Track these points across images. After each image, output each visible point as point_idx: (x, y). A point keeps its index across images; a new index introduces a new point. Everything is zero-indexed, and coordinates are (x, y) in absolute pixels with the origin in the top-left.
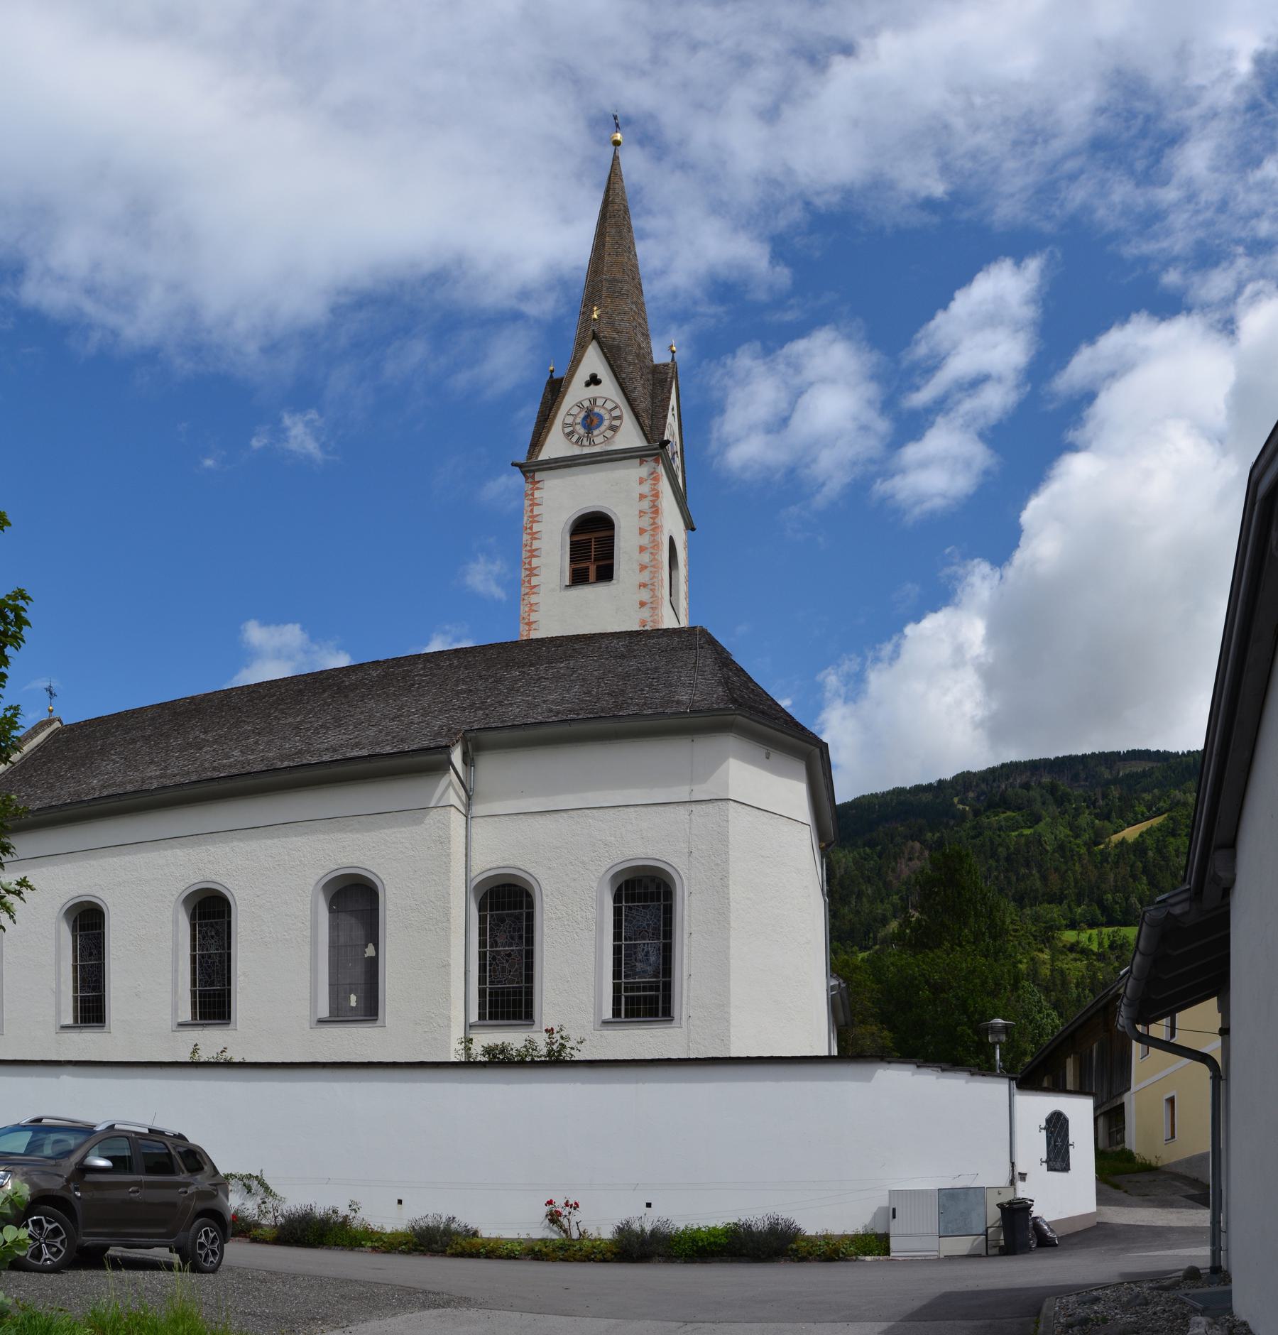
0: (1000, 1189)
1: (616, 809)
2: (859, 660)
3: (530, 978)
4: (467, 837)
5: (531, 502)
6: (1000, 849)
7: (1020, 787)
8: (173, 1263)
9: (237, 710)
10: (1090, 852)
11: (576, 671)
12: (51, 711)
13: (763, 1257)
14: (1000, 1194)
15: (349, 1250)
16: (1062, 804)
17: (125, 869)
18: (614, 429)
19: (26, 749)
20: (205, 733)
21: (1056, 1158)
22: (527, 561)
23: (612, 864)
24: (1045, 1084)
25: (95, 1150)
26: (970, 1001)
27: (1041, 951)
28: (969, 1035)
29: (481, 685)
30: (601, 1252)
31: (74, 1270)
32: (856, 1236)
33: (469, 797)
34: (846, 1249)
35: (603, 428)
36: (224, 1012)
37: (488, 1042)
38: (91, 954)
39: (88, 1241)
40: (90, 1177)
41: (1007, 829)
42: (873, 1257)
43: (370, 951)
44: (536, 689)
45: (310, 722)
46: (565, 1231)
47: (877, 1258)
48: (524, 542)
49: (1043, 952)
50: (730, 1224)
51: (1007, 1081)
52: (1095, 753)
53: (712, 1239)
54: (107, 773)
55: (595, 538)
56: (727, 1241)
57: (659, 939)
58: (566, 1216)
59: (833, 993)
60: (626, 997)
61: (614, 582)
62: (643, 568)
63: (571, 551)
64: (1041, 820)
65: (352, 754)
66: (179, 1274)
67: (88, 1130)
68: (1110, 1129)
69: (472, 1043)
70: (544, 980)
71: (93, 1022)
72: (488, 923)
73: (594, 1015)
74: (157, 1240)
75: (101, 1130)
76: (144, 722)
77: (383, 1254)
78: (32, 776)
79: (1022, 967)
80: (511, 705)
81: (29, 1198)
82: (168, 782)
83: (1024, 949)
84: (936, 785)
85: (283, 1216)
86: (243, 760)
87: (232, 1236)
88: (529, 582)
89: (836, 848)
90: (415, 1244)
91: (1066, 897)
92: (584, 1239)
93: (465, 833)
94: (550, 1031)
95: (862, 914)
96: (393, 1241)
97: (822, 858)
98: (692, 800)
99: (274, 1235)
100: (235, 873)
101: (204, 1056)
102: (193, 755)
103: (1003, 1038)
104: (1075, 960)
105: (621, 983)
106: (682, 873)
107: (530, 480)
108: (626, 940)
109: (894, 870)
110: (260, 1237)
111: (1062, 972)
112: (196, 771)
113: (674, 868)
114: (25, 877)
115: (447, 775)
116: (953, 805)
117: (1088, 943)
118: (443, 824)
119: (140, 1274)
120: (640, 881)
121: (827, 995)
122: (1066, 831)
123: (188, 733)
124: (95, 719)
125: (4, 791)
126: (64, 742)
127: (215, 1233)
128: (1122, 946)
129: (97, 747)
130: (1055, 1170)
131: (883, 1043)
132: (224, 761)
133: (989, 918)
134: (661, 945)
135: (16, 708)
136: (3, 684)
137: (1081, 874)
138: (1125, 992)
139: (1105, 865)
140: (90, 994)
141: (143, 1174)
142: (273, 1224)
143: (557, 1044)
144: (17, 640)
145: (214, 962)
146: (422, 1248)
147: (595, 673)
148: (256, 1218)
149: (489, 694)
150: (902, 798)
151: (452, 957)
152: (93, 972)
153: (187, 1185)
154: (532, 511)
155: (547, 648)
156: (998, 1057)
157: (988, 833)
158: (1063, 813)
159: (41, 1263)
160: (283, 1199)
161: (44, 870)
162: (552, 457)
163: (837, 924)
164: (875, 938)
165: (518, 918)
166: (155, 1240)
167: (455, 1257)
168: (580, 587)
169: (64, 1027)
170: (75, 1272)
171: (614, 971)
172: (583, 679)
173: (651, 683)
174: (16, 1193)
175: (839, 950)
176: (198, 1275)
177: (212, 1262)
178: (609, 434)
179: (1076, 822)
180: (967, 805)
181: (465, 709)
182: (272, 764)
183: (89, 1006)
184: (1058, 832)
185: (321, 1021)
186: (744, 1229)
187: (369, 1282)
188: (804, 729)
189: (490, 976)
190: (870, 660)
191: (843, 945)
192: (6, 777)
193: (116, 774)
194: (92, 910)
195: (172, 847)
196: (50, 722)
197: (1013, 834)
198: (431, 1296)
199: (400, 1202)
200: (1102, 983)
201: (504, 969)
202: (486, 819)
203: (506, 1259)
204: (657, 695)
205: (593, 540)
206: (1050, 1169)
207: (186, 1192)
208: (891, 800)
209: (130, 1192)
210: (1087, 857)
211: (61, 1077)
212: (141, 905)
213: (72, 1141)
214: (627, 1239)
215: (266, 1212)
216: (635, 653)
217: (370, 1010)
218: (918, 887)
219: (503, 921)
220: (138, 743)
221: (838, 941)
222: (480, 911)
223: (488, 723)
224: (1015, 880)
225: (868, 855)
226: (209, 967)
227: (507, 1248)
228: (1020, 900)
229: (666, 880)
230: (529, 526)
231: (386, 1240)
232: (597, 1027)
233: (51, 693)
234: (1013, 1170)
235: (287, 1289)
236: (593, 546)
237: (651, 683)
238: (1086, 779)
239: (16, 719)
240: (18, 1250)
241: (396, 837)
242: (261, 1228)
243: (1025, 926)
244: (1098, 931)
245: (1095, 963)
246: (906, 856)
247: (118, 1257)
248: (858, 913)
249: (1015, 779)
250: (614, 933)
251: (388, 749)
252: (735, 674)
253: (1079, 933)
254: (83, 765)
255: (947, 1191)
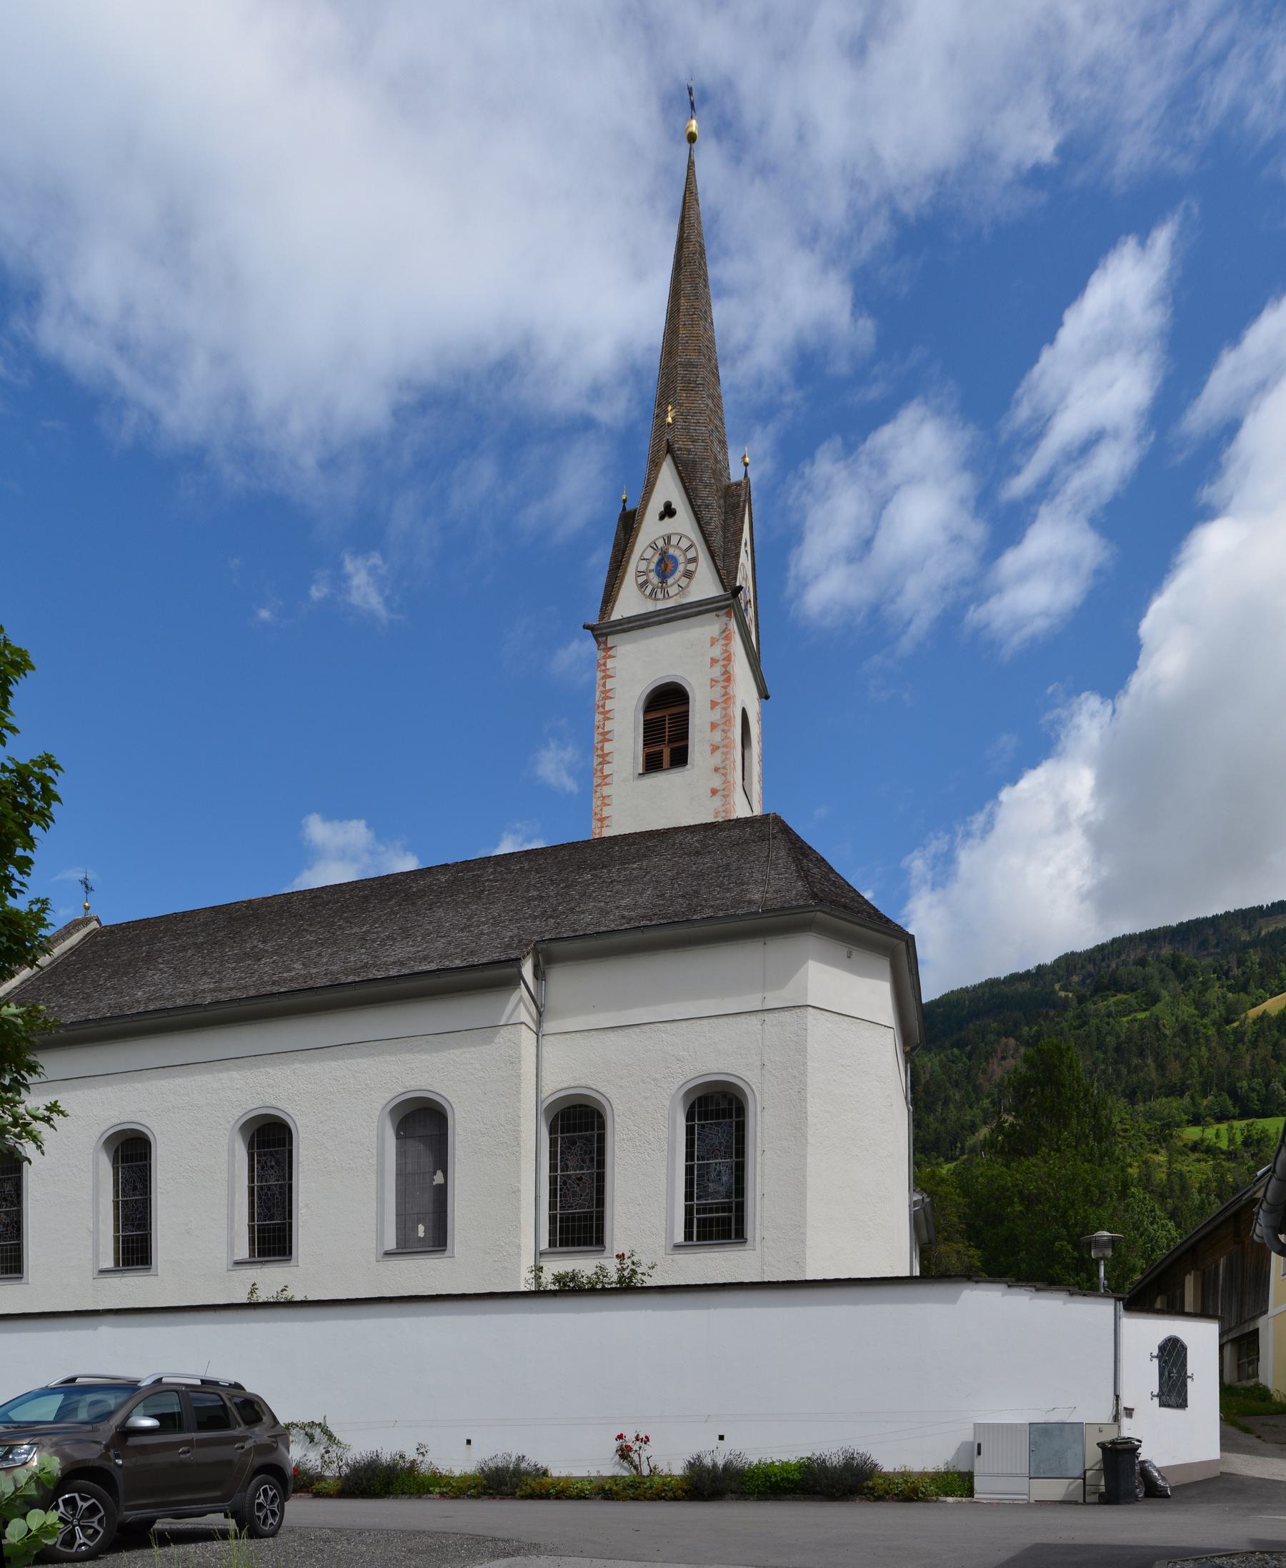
0: (1101, 1426)
1: (690, 1022)
2: (947, 837)
3: (601, 1202)
4: (537, 1055)
5: (604, 674)
6: (1108, 1038)
7: (1134, 964)
8: (228, 1530)
9: (299, 917)
10: (1219, 1032)
11: (649, 872)
12: (87, 908)
13: (837, 1495)
14: (1101, 1431)
15: (417, 1498)
16: (1186, 979)
17: (174, 1093)
18: (689, 575)
19: (57, 951)
20: (264, 942)
21: (1170, 1391)
22: (599, 746)
23: (684, 1081)
24: (1158, 1305)
25: (140, 1409)
26: (1071, 1213)
27: (1156, 1152)
28: (1067, 1250)
29: (553, 891)
30: (672, 1490)
31: (114, 1553)
32: (937, 1473)
33: (540, 1014)
34: (925, 1488)
35: (677, 575)
36: (285, 1248)
37: (558, 1269)
38: (135, 1188)
39: (131, 1516)
40: (133, 1441)
41: (1117, 1015)
42: (955, 1498)
43: (439, 1179)
44: (608, 894)
45: (377, 933)
46: (636, 1468)
47: (959, 1499)
48: (597, 724)
49: (1158, 1153)
50: (803, 1458)
51: (1112, 1301)
52: (1229, 912)
53: (785, 1475)
54: (154, 985)
55: (669, 715)
56: (800, 1477)
57: (731, 1157)
58: (636, 1451)
59: (916, 1208)
60: (698, 1219)
61: (688, 766)
62: (715, 748)
63: (644, 733)
64: (1160, 1001)
65: (420, 968)
66: (235, 1542)
67: (131, 1387)
68: (1239, 1360)
69: (542, 1272)
70: (616, 1204)
71: (137, 1264)
72: (559, 1145)
73: (666, 1238)
74: (211, 1505)
75: (146, 1386)
76: (196, 927)
77: (453, 1501)
78: (64, 984)
79: (1133, 1172)
80: (583, 912)
81: (59, 1473)
82: (223, 997)
83: (1135, 1151)
84: (1034, 971)
85: (347, 1465)
86: (305, 974)
87: (293, 1493)
88: (602, 770)
89: (921, 1051)
90: (485, 1487)
91: (1188, 1088)
92: (654, 1476)
93: (535, 1052)
94: (621, 1257)
95: (949, 1121)
96: (461, 1485)
97: (906, 1063)
98: (764, 1009)
99: (338, 1487)
100: (296, 1098)
101: (262, 1296)
102: (251, 967)
103: (1109, 1253)
104: (1199, 1161)
105: (693, 1205)
106: (754, 1087)
107: (602, 646)
108: (698, 1160)
109: (984, 1072)
110: (324, 1490)
111: (1181, 1175)
112: (253, 985)
113: (746, 1082)
114: (56, 1102)
115: (518, 990)
116: (1054, 992)
117: (1214, 1140)
118: (514, 1043)
119: (191, 1548)
120: (712, 1097)
121: (910, 1211)
122: (1190, 1010)
123: (245, 941)
124: (139, 921)
125: (30, 1000)
126: (103, 945)
127: (275, 1491)
128: (1259, 1141)
129: (142, 953)
130: (1169, 1406)
131: (970, 1262)
132: (285, 975)
133: (1094, 1117)
134: (734, 1164)
135: (45, 902)
136: (28, 871)
137: (1208, 1059)
138: (1265, 1196)
139: (1240, 1045)
140: (135, 1233)
141: (194, 1432)
142: (337, 1475)
143: (628, 1270)
144: (45, 818)
145: (274, 1194)
146: (491, 1491)
147: (669, 873)
148: (319, 1470)
149: (561, 901)
150: (996, 990)
151: (522, 1182)
152: (137, 1209)
153: (245, 1439)
154: (604, 685)
155: (620, 847)
156: (1102, 1274)
157: (1094, 1021)
158: (1185, 990)
159: (74, 1550)
160: (347, 1447)
161: (79, 1093)
162: (625, 616)
163: (921, 1134)
164: (963, 1148)
165: (590, 1140)
166: (208, 1505)
167: (525, 1499)
168: (654, 775)
169: (102, 1272)
170: (115, 1555)
171: (686, 1192)
172: (656, 881)
173: (722, 882)
174: (44, 1469)
175: (923, 1163)
176: (257, 1541)
177: (271, 1524)
178: (683, 582)
179: (1204, 998)
180: (1070, 992)
181: (536, 917)
182: (337, 979)
183: (133, 1247)
184: (1180, 1013)
185: (387, 1254)
186: (818, 1464)
187: (437, 1532)
188: (888, 921)
189: (561, 1201)
190: (960, 837)
191: (927, 1157)
192: (32, 983)
193: (164, 986)
194: (137, 1139)
195: (228, 1069)
196: (86, 921)
197: (1125, 1019)
198: (500, 1544)
199: (469, 1442)
200: (1231, 1187)
201: (574, 1194)
202: (557, 1036)
203: (576, 1499)
204: (728, 895)
205: (667, 718)
206: (1162, 1404)
207: (243, 1448)
208: (983, 993)
209: (180, 1453)
210: (1216, 1039)
211: (100, 1328)
212: (193, 1133)
213: (111, 1401)
214: (698, 1475)
215: (330, 1462)
216: (709, 849)
217: (439, 1240)
218: (1011, 1089)
219: (574, 1143)
220: (189, 951)
221: (921, 1153)
222: (550, 1133)
223: (559, 933)
224: (1126, 1073)
225: (955, 1056)
226: (269, 1199)
227: (577, 1488)
228: (1131, 1096)
229: (738, 1096)
230: (601, 703)
231: (454, 1485)
232: (669, 1251)
233: (87, 887)
234: (1117, 1404)
235: (352, 1547)
236: (667, 726)
237: (722, 882)
238: (1217, 946)
239: (44, 915)
240: (45, 1539)
241: (465, 1058)
242: (325, 1480)
243: (1137, 1125)
244: (1229, 1125)
245: (1224, 1163)
246: (999, 1055)
247: (166, 1530)
248: (944, 1121)
249: (1128, 955)
250: (687, 1152)
251: (458, 963)
252: (816, 865)
253: (1204, 1129)
254: (126, 974)
255: (1039, 1425)
